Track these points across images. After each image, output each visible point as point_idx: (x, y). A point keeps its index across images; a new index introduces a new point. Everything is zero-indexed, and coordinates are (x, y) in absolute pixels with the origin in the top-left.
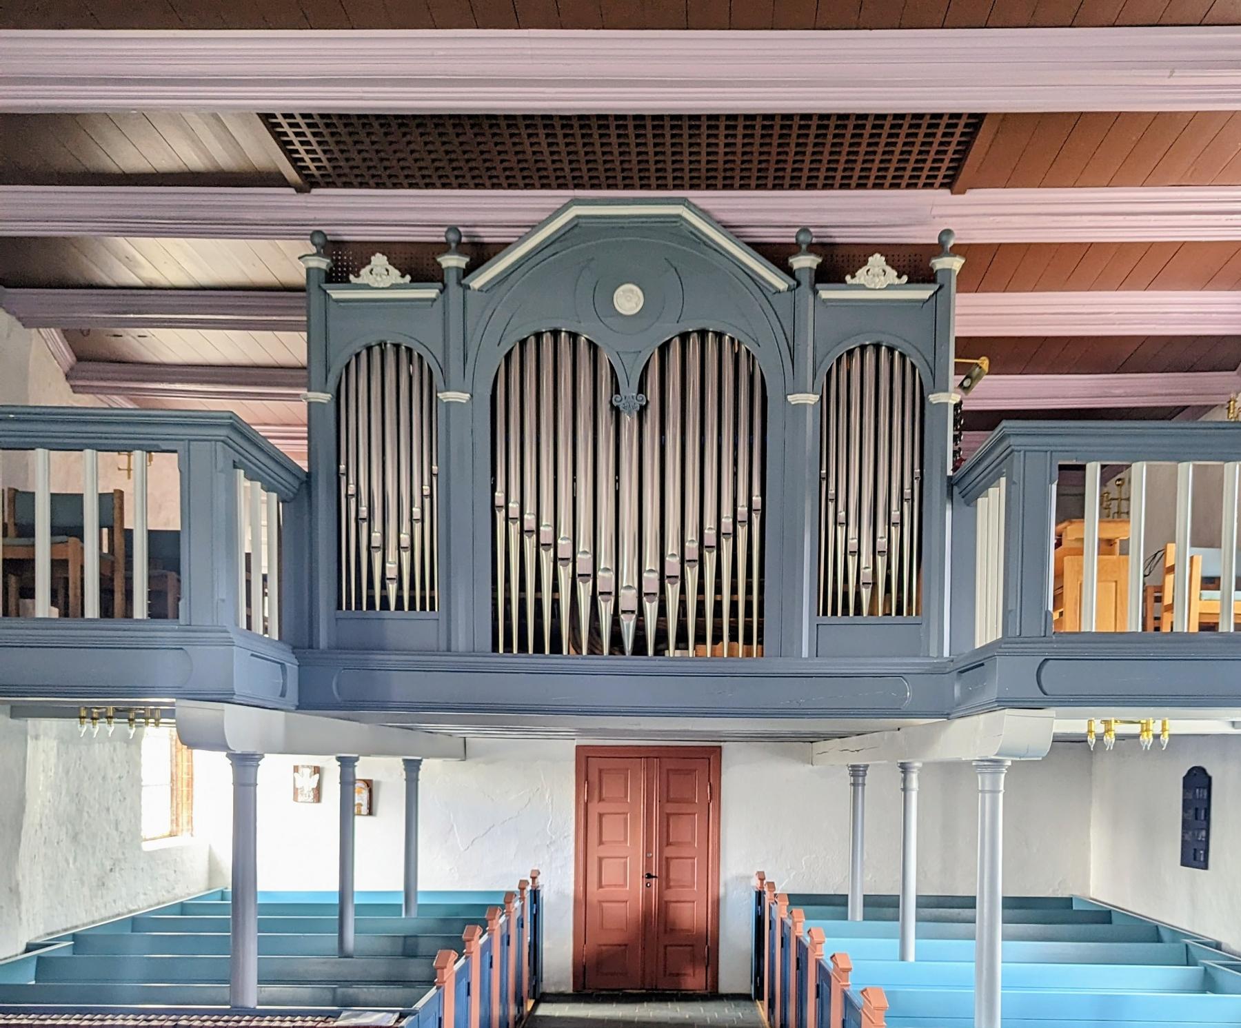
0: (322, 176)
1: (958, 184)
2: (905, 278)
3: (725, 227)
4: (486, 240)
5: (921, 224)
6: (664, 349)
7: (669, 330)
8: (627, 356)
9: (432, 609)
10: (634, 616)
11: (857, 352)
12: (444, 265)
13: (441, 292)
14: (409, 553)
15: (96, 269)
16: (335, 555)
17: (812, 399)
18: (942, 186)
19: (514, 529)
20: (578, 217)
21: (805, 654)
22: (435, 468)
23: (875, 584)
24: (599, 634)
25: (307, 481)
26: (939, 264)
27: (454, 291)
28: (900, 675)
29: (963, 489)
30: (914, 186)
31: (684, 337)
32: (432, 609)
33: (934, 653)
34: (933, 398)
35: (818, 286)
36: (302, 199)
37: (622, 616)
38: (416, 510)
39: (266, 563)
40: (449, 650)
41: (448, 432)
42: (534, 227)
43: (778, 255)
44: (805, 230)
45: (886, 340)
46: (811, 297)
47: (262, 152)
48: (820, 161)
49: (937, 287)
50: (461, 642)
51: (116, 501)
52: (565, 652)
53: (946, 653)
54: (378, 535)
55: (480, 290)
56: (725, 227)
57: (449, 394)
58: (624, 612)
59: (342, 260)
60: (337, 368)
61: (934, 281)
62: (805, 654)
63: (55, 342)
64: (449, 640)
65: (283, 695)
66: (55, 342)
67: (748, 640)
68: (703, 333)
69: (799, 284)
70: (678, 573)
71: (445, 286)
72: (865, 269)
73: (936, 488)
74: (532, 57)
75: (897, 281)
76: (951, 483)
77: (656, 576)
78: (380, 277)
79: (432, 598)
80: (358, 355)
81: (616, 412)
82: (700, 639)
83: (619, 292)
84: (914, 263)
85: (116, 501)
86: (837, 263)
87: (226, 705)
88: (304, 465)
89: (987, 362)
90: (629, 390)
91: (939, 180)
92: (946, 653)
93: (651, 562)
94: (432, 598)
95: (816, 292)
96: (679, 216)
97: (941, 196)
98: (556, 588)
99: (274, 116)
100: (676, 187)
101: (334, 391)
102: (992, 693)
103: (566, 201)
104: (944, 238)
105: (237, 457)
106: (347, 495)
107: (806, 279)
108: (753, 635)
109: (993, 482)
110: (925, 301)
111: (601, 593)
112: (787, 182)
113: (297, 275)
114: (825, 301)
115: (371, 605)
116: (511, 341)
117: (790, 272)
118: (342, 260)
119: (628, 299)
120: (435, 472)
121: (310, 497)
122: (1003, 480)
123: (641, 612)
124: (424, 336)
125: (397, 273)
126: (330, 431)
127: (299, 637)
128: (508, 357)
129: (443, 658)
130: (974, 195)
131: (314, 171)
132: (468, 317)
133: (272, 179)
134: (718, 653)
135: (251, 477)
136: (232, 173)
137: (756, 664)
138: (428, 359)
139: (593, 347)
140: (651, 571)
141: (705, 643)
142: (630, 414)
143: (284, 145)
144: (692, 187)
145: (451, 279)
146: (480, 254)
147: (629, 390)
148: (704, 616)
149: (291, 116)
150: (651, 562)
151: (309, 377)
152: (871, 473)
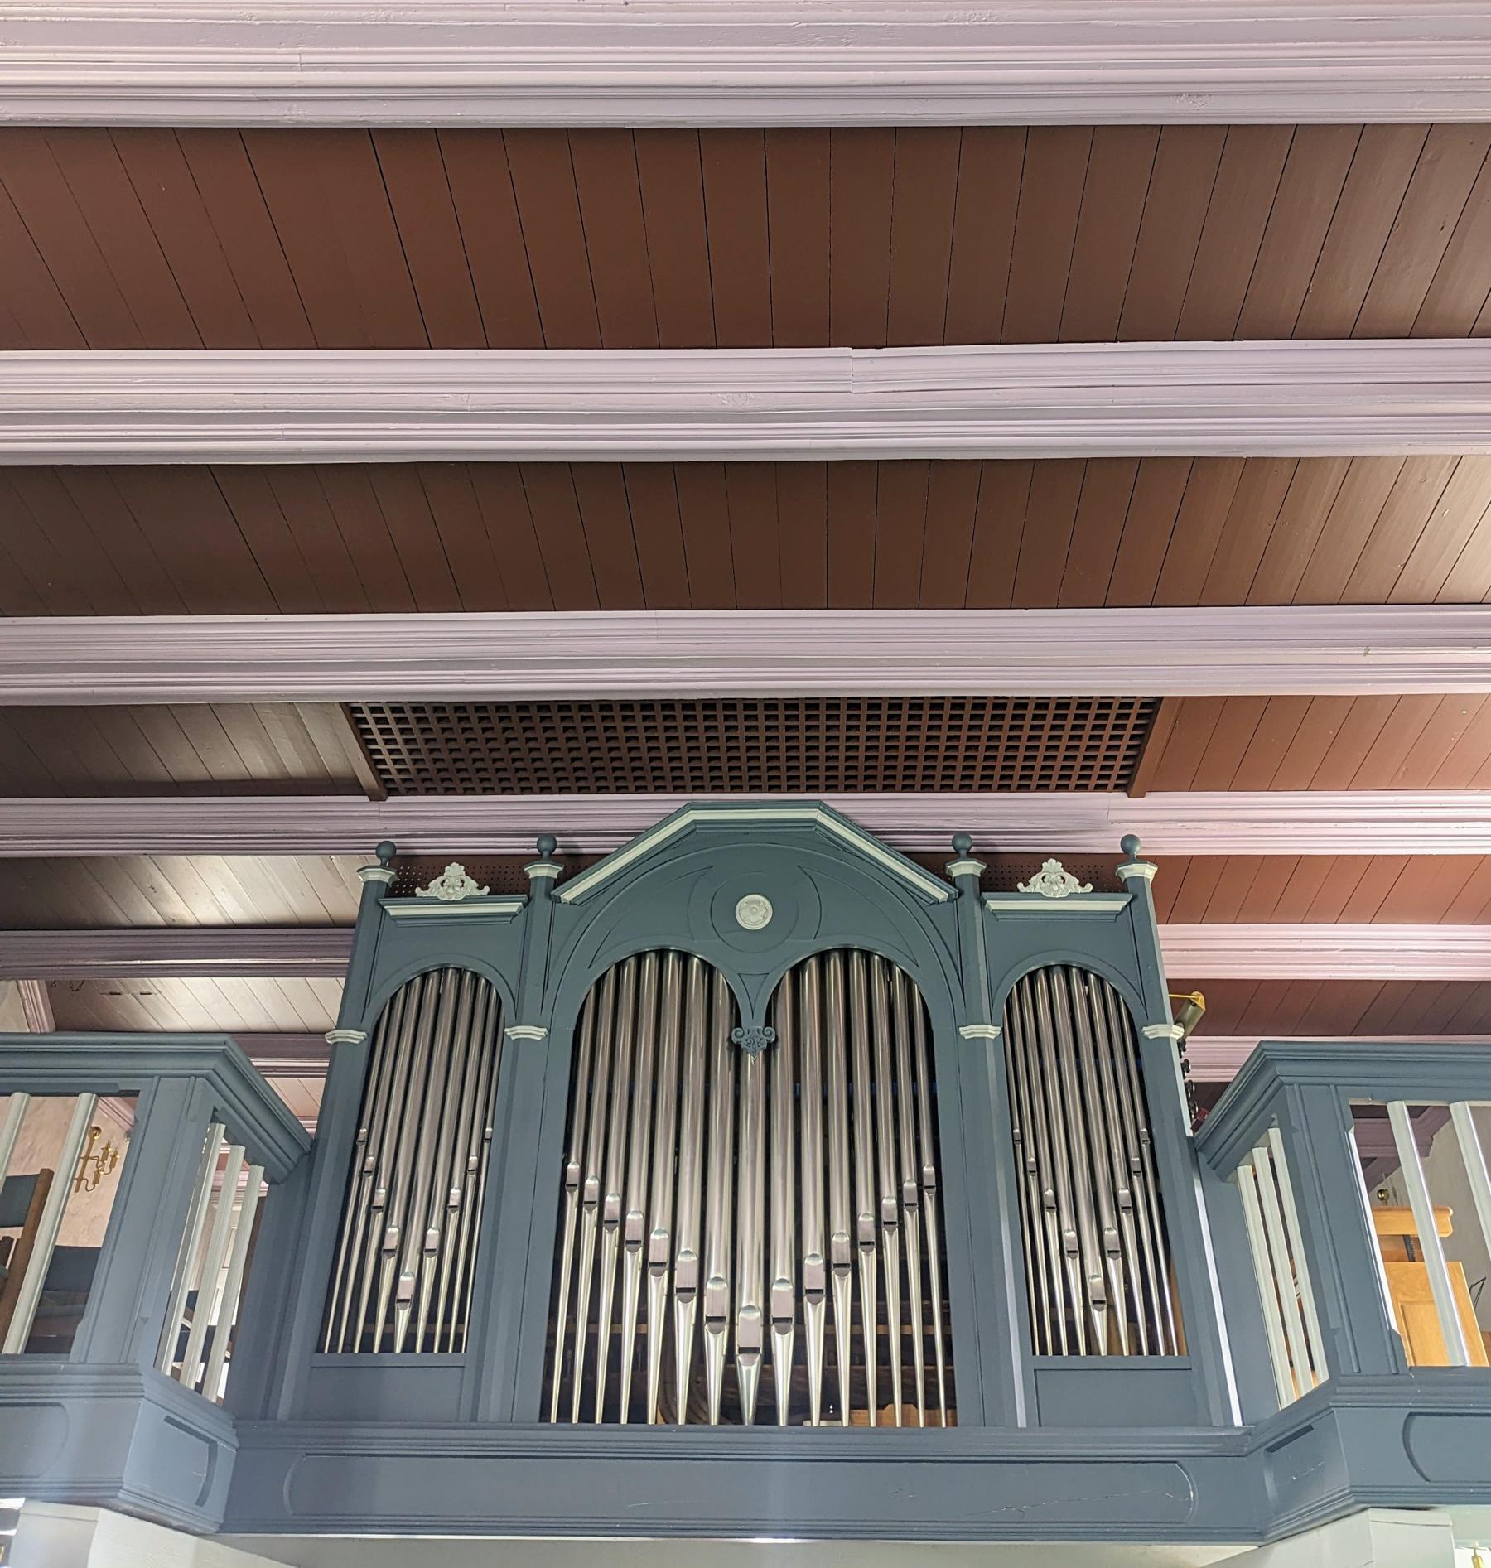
0: (404, 780)
1: (1135, 787)
2: (1089, 887)
3: (873, 834)
4: (585, 851)
5: (1096, 829)
6: (797, 971)
7: (803, 948)
8: (749, 981)
9: (457, 1348)
10: (758, 1358)
11: (1042, 974)
12: (532, 876)
13: (525, 906)
14: (434, 1259)
15: (105, 897)
16: (332, 1246)
17: (991, 1032)
18: (1117, 787)
19: (590, 1219)
20: (695, 822)
21: (1022, 1421)
22: (488, 1129)
23: (1111, 1308)
24: (705, 1396)
25: (311, 1151)
26: (1130, 871)
27: (541, 904)
28: (1174, 1460)
29: (1215, 1157)
30: (1084, 788)
31: (823, 957)
32: (457, 1348)
33: (1217, 1420)
34: (1149, 1032)
35: (985, 894)
36: (375, 808)
37: (740, 1358)
38: (455, 1193)
39: (219, 1309)
40: (474, 1419)
41: (511, 1089)
42: (638, 835)
43: (933, 863)
44: (964, 835)
45: (1076, 960)
46: (977, 908)
47: (339, 752)
48: (973, 767)
49: (1129, 897)
50: (493, 1405)
51: (39, 1187)
52: (651, 1421)
53: (1238, 1422)
54: (396, 1230)
55: (572, 903)
56: (873, 834)
57: (519, 1029)
58: (743, 1350)
59: (410, 873)
60: (380, 999)
61: (1125, 891)
62: (1022, 1421)
63: (36, 1010)
64: (475, 1408)
65: (201, 1502)
66: (36, 1010)
67: (931, 1404)
68: (846, 953)
69: (961, 894)
70: (822, 1286)
71: (530, 899)
72: (1039, 876)
73: (1174, 1159)
74: (657, 637)
75: (1080, 890)
76: (1194, 1148)
77: (789, 1288)
78: (454, 889)
79: (458, 1336)
80: (409, 984)
81: (737, 1051)
82: (859, 1401)
83: (743, 903)
84: (1098, 872)
85: (39, 1187)
86: (1005, 872)
87: (102, 1511)
88: (310, 1126)
89: (1202, 997)
90: (753, 1022)
91: (1113, 781)
92: (1238, 1422)
93: (782, 1268)
94: (458, 1336)
95: (983, 903)
96: (814, 821)
97: (1119, 798)
98: (642, 1318)
99: (359, 710)
100: (809, 789)
101: (371, 1031)
102: (1338, 1480)
103: (680, 805)
104: (1128, 844)
105: (221, 1104)
106: (362, 1171)
107: (970, 889)
108: (940, 1395)
109: (1256, 1137)
110: (1118, 914)
111: (710, 1319)
112: (937, 783)
113: (346, 904)
114: (994, 913)
115: (367, 1346)
116: (605, 964)
117: (949, 880)
118: (410, 873)
119: (754, 913)
120: (487, 1136)
121: (310, 1175)
122: (1275, 1134)
123: (768, 1358)
124: (493, 961)
125: (474, 884)
126: (357, 1096)
127: (249, 1408)
128: (599, 984)
129: (462, 1433)
130: (1153, 799)
131: (395, 775)
132: (555, 937)
133: (347, 785)
134: (885, 1421)
135: (232, 1139)
136: (301, 779)
137: (947, 1438)
138: (498, 987)
139: (709, 970)
140: (782, 1281)
141: (866, 1407)
142: (754, 1054)
143: (366, 743)
144: (828, 789)
145: (538, 892)
146: (575, 864)
147: (753, 1022)
148: (863, 1362)
149: (380, 710)
150: (782, 1268)
151: (355, 942)
152: (1081, 1138)
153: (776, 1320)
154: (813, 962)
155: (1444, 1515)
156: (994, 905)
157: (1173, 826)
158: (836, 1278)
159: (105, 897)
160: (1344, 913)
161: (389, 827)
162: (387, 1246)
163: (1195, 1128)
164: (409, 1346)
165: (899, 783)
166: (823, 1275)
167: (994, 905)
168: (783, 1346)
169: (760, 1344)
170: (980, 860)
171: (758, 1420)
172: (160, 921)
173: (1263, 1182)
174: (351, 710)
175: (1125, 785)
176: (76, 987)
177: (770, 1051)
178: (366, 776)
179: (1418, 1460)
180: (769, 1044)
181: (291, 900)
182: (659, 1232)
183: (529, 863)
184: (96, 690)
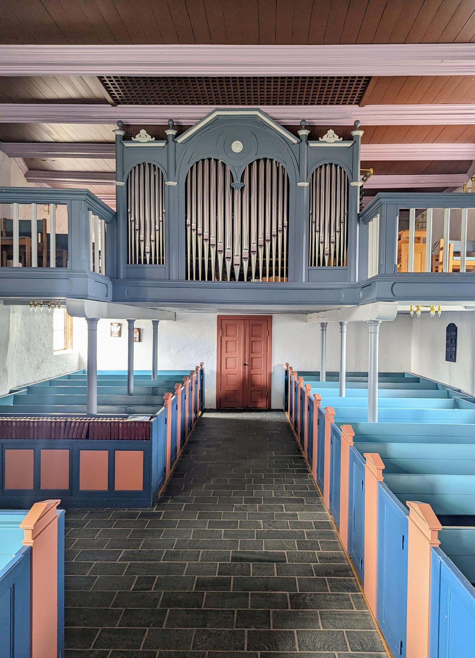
0: (122, 100)
1: (362, 103)
2: (341, 139)
3: (274, 119)
6: (250, 165)
7: (252, 158)
8: (237, 168)
9: (163, 264)
11: (324, 167)
12: (167, 134)
13: (166, 144)
14: (154, 242)
15: (32, 132)
17: (306, 184)
18: (356, 104)
20: (218, 115)
21: (304, 281)
22: (164, 210)
24: (226, 273)
25: (116, 215)
26: (354, 133)
27: (171, 143)
28: (340, 289)
31: (258, 161)
32: (163, 264)
34: (352, 184)
35: (309, 142)
36: (114, 109)
37: (235, 266)
38: (157, 226)
40: (169, 279)
43: (293, 130)
44: (304, 120)
45: (334, 162)
46: (306, 146)
47: (99, 91)
51: (44, 223)
52: (213, 280)
53: (357, 280)
55: (181, 143)
56: (274, 119)
57: (169, 182)
58: (235, 265)
59: (129, 132)
60: (127, 173)
61: (352, 140)
62: (304, 281)
65: (107, 296)
66: (22, 165)
67: (282, 275)
68: (265, 160)
69: (301, 141)
70: (256, 250)
72: (326, 135)
73: (353, 218)
74: (201, 55)
75: (338, 140)
76: (359, 216)
77: (247, 251)
78: (143, 138)
79: (163, 260)
80: (135, 168)
81: (233, 189)
82: (264, 275)
84: (345, 133)
85: (44, 223)
86: (316, 133)
88: (115, 209)
90: (237, 181)
92: (357, 280)
94: (163, 260)
95: (308, 144)
96: (256, 115)
98: (210, 256)
99: (103, 77)
100: (255, 104)
102: (374, 295)
103: (213, 109)
104: (356, 124)
105: (89, 206)
107: (304, 139)
108: (284, 274)
110: (349, 147)
111: (227, 258)
112: (297, 102)
114: (311, 147)
115: (140, 262)
116: (193, 162)
117: (298, 136)
118: (129, 132)
119: (237, 147)
122: (379, 215)
124: (160, 161)
125: (150, 136)
126: (124, 196)
127: (113, 274)
128: (192, 169)
131: (118, 98)
133: (102, 101)
134: (271, 280)
135: (94, 214)
137: (285, 284)
139: (224, 165)
140: (246, 249)
141: (266, 276)
142: (238, 190)
143: (107, 88)
144: (261, 104)
145: (170, 139)
146: (181, 129)
147: (237, 181)
149: (110, 77)
150: (245, 246)
152: (329, 212)
153: (244, 258)
154: (255, 162)
155: (397, 303)
156: (311, 145)
157: (372, 116)
158: (259, 249)
159: (32, 132)
160: (424, 141)
161: (120, 115)
162: (141, 239)
163: (360, 211)
164: (151, 262)
165: (284, 103)
166: (256, 248)
167: (311, 145)
168: (246, 264)
169: (240, 263)
170: (309, 130)
171: (239, 280)
172: (52, 140)
173: (374, 225)
174: (101, 78)
175: (358, 103)
176: (32, 159)
177: (242, 189)
178: (109, 99)
179: (394, 292)
180: (242, 187)
181: (92, 135)
182: (212, 237)
183: (166, 129)
184: (15, 72)
